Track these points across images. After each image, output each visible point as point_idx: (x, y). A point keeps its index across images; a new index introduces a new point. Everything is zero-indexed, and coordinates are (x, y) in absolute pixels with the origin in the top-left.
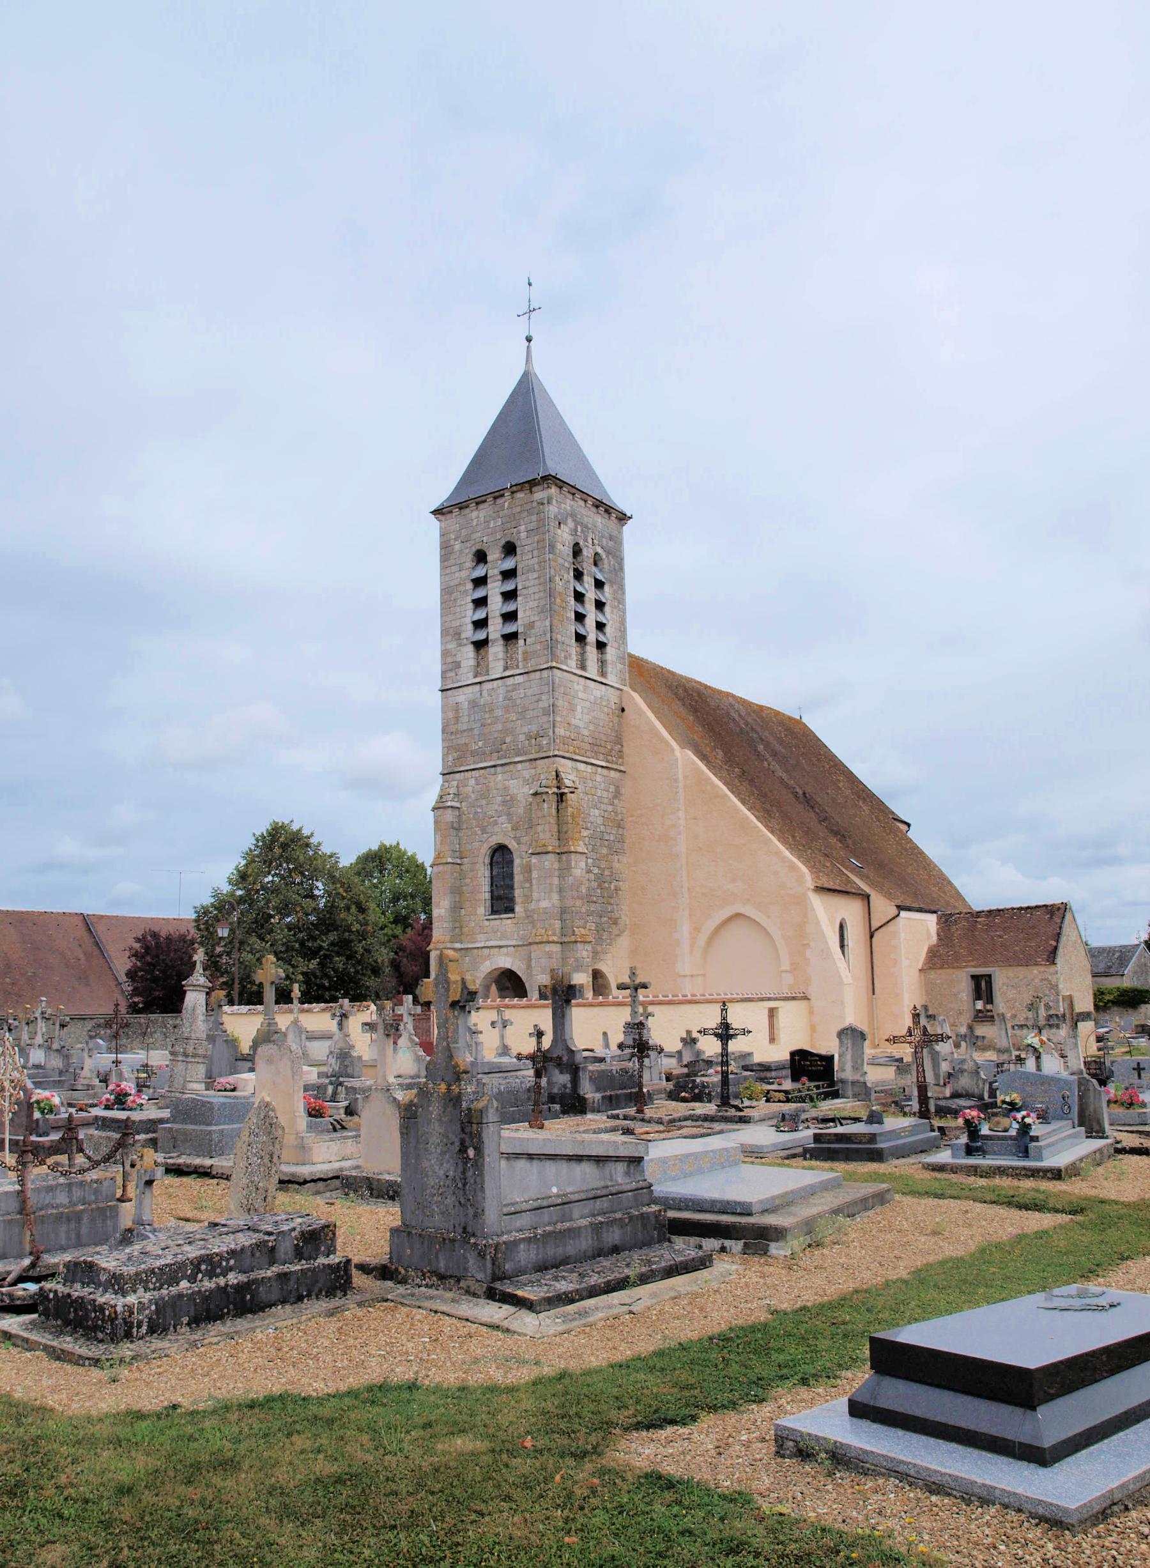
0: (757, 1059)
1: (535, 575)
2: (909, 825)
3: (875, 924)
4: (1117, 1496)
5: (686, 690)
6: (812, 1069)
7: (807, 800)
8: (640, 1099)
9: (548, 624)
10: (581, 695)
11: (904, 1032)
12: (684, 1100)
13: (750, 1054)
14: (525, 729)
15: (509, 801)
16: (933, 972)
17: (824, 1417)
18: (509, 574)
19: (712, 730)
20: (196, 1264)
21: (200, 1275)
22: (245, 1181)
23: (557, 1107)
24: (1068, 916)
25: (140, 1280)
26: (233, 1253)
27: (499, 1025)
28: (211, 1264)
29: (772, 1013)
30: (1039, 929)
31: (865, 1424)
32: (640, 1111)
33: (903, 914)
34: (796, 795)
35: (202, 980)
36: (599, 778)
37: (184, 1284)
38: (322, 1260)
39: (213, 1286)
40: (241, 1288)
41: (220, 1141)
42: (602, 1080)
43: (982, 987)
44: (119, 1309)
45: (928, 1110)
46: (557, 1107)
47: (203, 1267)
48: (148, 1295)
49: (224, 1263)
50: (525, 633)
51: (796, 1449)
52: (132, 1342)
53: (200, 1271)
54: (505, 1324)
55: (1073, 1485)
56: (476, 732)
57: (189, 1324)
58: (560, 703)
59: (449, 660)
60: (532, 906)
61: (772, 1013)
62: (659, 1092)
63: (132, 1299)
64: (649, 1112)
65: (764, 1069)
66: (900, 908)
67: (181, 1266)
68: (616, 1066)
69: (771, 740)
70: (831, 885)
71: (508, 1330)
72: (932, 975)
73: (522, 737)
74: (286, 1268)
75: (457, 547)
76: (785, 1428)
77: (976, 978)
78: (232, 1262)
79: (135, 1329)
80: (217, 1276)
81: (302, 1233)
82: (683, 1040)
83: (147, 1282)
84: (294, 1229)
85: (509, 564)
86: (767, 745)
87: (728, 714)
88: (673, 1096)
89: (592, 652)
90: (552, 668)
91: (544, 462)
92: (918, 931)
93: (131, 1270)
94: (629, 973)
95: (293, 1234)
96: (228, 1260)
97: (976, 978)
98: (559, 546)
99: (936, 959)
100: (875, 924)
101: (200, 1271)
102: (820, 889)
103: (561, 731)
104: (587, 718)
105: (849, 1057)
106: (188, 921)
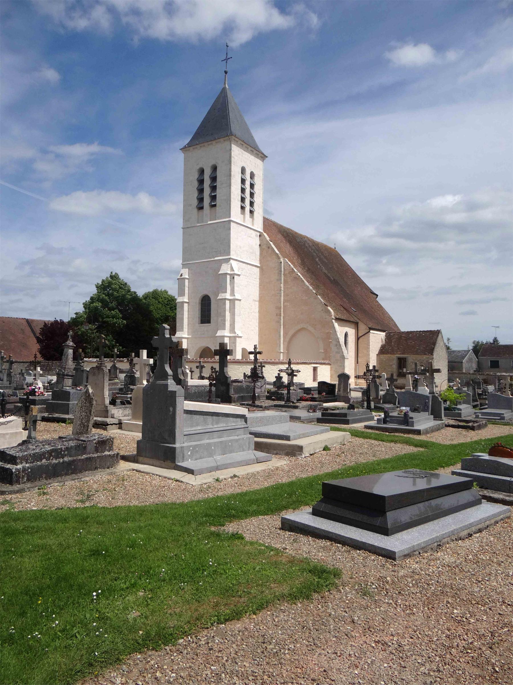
0: (306, 386)
2: (377, 295)
3: (360, 335)
4: (416, 549)
5: (287, 233)
6: (326, 390)
7: (335, 283)
8: (254, 398)
11: (362, 374)
12: (273, 400)
13: (303, 384)
16: (382, 355)
17: (303, 516)
19: (297, 251)
20: (50, 453)
21: (52, 458)
22: (79, 422)
23: (220, 400)
24: (440, 336)
25: (25, 459)
26: (67, 449)
27: (200, 367)
28: (57, 453)
29: (315, 369)
30: (428, 340)
31: (318, 519)
32: (254, 402)
33: (371, 331)
34: (330, 279)
35: (71, 344)
37: (44, 461)
38: (107, 453)
39: (57, 462)
40: (70, 463)
41: (72, 408)
42: (239, 390)
43: (402, 363)
44: (14, 471)
45: (370, 407)
46: (220, 400)
47: (53, 454)
48: (27, 465)
49: (63, 453)
51: (289, 526)
52: (19, 484)
53: (51, 455)
54: (181, 479)
55: (395, 543)
57: (45, 478)
60: (356, 386)
61: (315, 369)
62: (264, 396)
63: (19, 467)
64: (257, 403)
65: (308, 391)
66: (371, 329)
67: (44, 454)
68: (244, 385)
69: (322, 257)
70: (343, 318)
71: (182, 482)
72: (382, 356)
74: (91, 455)
76: (286, 519)
77: (400, 359)
78: (66, 452)
79: (21, 479)
80: (59, 458)
81: (99, 441)
82: (276, 377)
83: (27, 460)
84: (95, 439)
86: (320, 259)
87: (304, 245)
88: (268, 398)
91: (230, 129)
92: (377, 339)
93: (21, 454)
94: (254, 347)
95: (94, 442)
96: (64, 451)
97: (400, 359)
99: (383, 351)
100: (360, 335)
101: (51, 455)
102: (337, 319)
105: (342, 386)
106: (373, 487)
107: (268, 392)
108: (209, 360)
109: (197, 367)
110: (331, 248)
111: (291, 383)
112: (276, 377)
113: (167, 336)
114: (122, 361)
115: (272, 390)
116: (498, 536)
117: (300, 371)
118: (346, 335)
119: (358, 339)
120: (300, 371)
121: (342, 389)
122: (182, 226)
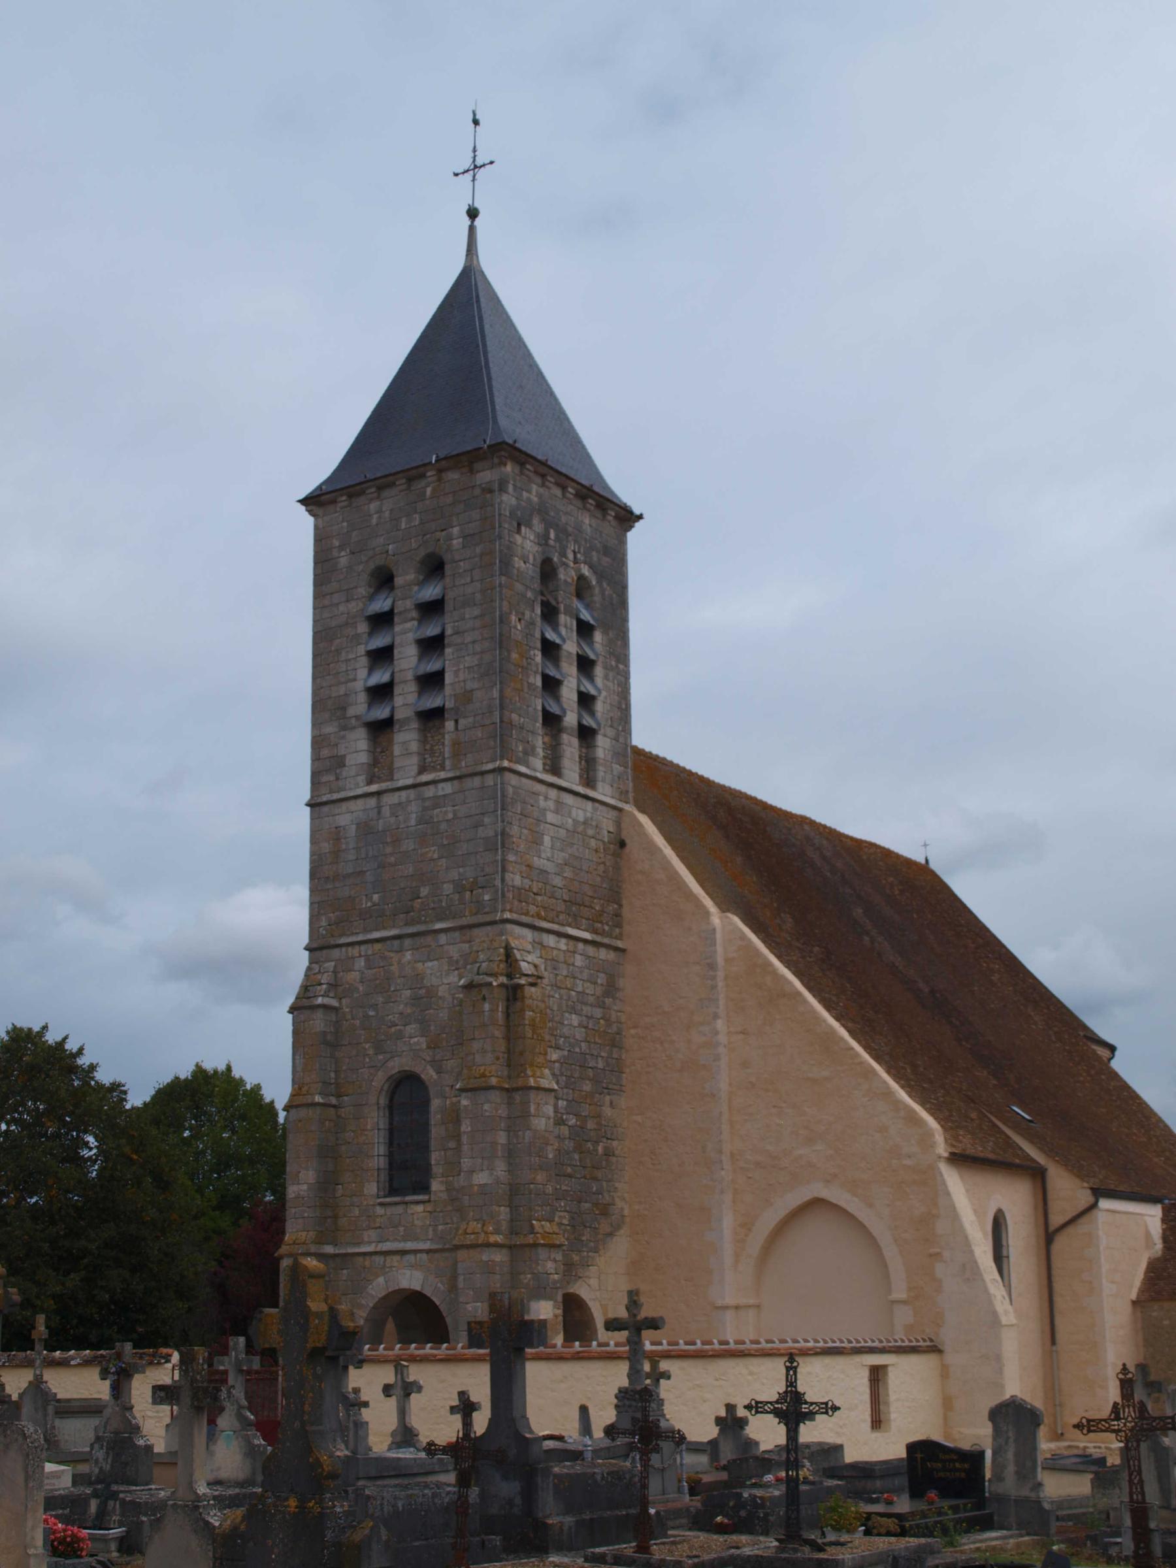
1: (476, 611)
2: (1112, 1049)
3: (1056, 1220)
9: (495, 693)
10: (551, 817)
13: (838, 1448)
14: (454, 875)
15: (424, 998)
18: (432, 609)
23: (497, 1540)
27: (398, 1391)
29: (877, 1375)
33: (1104, 1204)
36: (579, 961)
46: (497, 1540)
50: (456, 710)
56: (369, 877)
58: (515, 830)
59: (325, 752)
61: (877, 1375)
66: (1099, 1193)
68: (601, 1467)
73: (448, 888)
75: (343, 561)
82: (719, 1421)
85: (430, 592)
88: (701, 1522)
89: (571, 746)
90: (501, 770)
98: (518, 563)
100: (1056, 1220)
102: (958, 1159)
103: (516, 879)
104: (560, 857)
105: (1010, 1455)
107: (693, 1492)
108: (428, 1349)
109: (387, 1390)
110: (909, 863)
111: (793, 1449)
112: (719, 1421)
113: (95, 1151)
114: (63, 1364)
115: (706, 1479)
116: (595, 810)
117: (835, 1408)
118: (998, 1224)
119: (1049, 1236)
120: (835, 1408)
121: (1011, 1469)
122: (307, 796)
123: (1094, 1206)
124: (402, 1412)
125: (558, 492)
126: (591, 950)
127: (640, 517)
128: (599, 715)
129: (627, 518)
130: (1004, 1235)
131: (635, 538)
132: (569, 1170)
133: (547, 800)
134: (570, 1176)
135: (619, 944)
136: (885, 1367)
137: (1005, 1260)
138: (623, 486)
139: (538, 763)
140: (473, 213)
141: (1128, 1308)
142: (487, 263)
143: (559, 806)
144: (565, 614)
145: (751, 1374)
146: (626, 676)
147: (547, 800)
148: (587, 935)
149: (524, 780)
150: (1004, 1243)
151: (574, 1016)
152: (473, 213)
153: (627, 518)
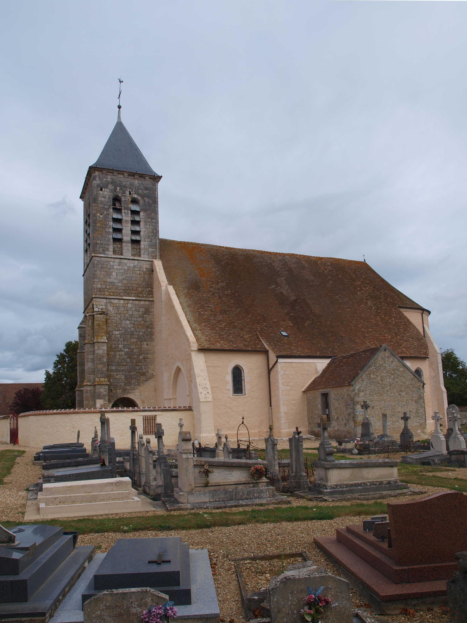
2: (425, 312)
33: (280, 360)
123: (277, 361)
124: (405, 424)
125: (122, 176)
126: (136, 302)
127: (161, 177)
128: (142, 236)
129: (157, 178)
130: (243, 373)
131: (161, 185)
132: (125, 364)
133: (115, 264)
134: (125, 365)
135: (151, 299)
136: (156, 415)
137: (243, 381)
138: (157, 171)
139: (111, 253)
140: (119, 107)
141: (301, 394)
142: (123, 121)
143: (120, 264)
144: (124, 209)
145: (80, 418)
146: (157, 223)
147: (115, 264)
148: (134, 298)
149: (102, 258)
150: (243, 376)
151: (127, 321)
152: (119, 107)
153: (157, 178)
